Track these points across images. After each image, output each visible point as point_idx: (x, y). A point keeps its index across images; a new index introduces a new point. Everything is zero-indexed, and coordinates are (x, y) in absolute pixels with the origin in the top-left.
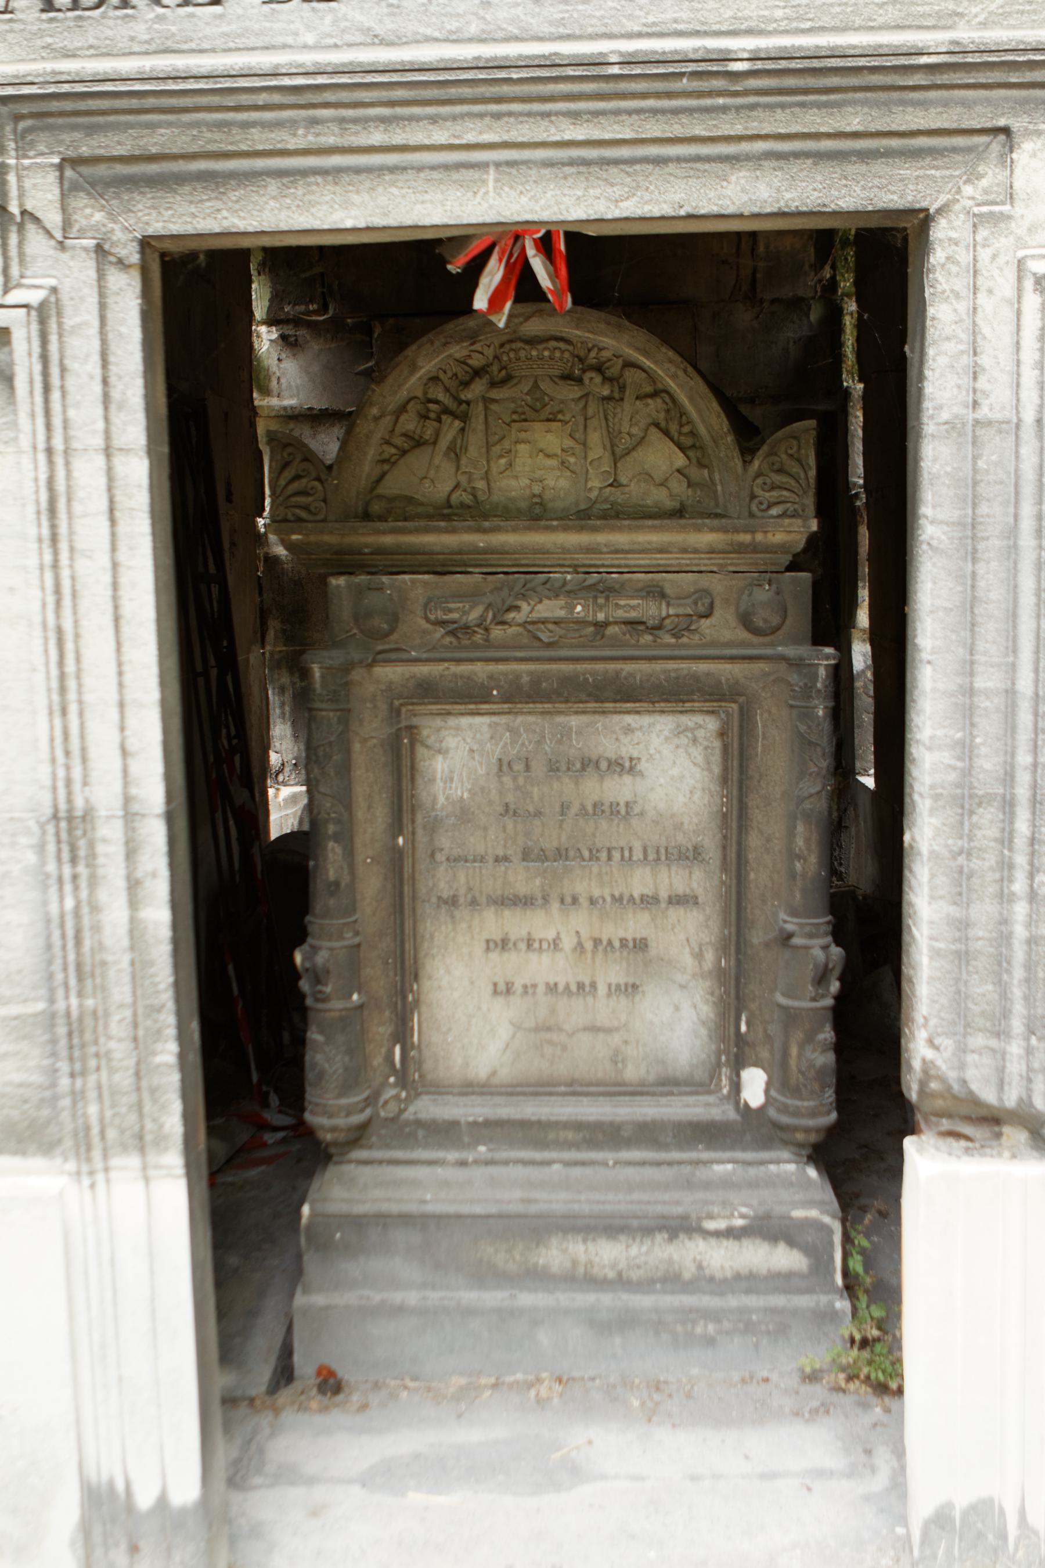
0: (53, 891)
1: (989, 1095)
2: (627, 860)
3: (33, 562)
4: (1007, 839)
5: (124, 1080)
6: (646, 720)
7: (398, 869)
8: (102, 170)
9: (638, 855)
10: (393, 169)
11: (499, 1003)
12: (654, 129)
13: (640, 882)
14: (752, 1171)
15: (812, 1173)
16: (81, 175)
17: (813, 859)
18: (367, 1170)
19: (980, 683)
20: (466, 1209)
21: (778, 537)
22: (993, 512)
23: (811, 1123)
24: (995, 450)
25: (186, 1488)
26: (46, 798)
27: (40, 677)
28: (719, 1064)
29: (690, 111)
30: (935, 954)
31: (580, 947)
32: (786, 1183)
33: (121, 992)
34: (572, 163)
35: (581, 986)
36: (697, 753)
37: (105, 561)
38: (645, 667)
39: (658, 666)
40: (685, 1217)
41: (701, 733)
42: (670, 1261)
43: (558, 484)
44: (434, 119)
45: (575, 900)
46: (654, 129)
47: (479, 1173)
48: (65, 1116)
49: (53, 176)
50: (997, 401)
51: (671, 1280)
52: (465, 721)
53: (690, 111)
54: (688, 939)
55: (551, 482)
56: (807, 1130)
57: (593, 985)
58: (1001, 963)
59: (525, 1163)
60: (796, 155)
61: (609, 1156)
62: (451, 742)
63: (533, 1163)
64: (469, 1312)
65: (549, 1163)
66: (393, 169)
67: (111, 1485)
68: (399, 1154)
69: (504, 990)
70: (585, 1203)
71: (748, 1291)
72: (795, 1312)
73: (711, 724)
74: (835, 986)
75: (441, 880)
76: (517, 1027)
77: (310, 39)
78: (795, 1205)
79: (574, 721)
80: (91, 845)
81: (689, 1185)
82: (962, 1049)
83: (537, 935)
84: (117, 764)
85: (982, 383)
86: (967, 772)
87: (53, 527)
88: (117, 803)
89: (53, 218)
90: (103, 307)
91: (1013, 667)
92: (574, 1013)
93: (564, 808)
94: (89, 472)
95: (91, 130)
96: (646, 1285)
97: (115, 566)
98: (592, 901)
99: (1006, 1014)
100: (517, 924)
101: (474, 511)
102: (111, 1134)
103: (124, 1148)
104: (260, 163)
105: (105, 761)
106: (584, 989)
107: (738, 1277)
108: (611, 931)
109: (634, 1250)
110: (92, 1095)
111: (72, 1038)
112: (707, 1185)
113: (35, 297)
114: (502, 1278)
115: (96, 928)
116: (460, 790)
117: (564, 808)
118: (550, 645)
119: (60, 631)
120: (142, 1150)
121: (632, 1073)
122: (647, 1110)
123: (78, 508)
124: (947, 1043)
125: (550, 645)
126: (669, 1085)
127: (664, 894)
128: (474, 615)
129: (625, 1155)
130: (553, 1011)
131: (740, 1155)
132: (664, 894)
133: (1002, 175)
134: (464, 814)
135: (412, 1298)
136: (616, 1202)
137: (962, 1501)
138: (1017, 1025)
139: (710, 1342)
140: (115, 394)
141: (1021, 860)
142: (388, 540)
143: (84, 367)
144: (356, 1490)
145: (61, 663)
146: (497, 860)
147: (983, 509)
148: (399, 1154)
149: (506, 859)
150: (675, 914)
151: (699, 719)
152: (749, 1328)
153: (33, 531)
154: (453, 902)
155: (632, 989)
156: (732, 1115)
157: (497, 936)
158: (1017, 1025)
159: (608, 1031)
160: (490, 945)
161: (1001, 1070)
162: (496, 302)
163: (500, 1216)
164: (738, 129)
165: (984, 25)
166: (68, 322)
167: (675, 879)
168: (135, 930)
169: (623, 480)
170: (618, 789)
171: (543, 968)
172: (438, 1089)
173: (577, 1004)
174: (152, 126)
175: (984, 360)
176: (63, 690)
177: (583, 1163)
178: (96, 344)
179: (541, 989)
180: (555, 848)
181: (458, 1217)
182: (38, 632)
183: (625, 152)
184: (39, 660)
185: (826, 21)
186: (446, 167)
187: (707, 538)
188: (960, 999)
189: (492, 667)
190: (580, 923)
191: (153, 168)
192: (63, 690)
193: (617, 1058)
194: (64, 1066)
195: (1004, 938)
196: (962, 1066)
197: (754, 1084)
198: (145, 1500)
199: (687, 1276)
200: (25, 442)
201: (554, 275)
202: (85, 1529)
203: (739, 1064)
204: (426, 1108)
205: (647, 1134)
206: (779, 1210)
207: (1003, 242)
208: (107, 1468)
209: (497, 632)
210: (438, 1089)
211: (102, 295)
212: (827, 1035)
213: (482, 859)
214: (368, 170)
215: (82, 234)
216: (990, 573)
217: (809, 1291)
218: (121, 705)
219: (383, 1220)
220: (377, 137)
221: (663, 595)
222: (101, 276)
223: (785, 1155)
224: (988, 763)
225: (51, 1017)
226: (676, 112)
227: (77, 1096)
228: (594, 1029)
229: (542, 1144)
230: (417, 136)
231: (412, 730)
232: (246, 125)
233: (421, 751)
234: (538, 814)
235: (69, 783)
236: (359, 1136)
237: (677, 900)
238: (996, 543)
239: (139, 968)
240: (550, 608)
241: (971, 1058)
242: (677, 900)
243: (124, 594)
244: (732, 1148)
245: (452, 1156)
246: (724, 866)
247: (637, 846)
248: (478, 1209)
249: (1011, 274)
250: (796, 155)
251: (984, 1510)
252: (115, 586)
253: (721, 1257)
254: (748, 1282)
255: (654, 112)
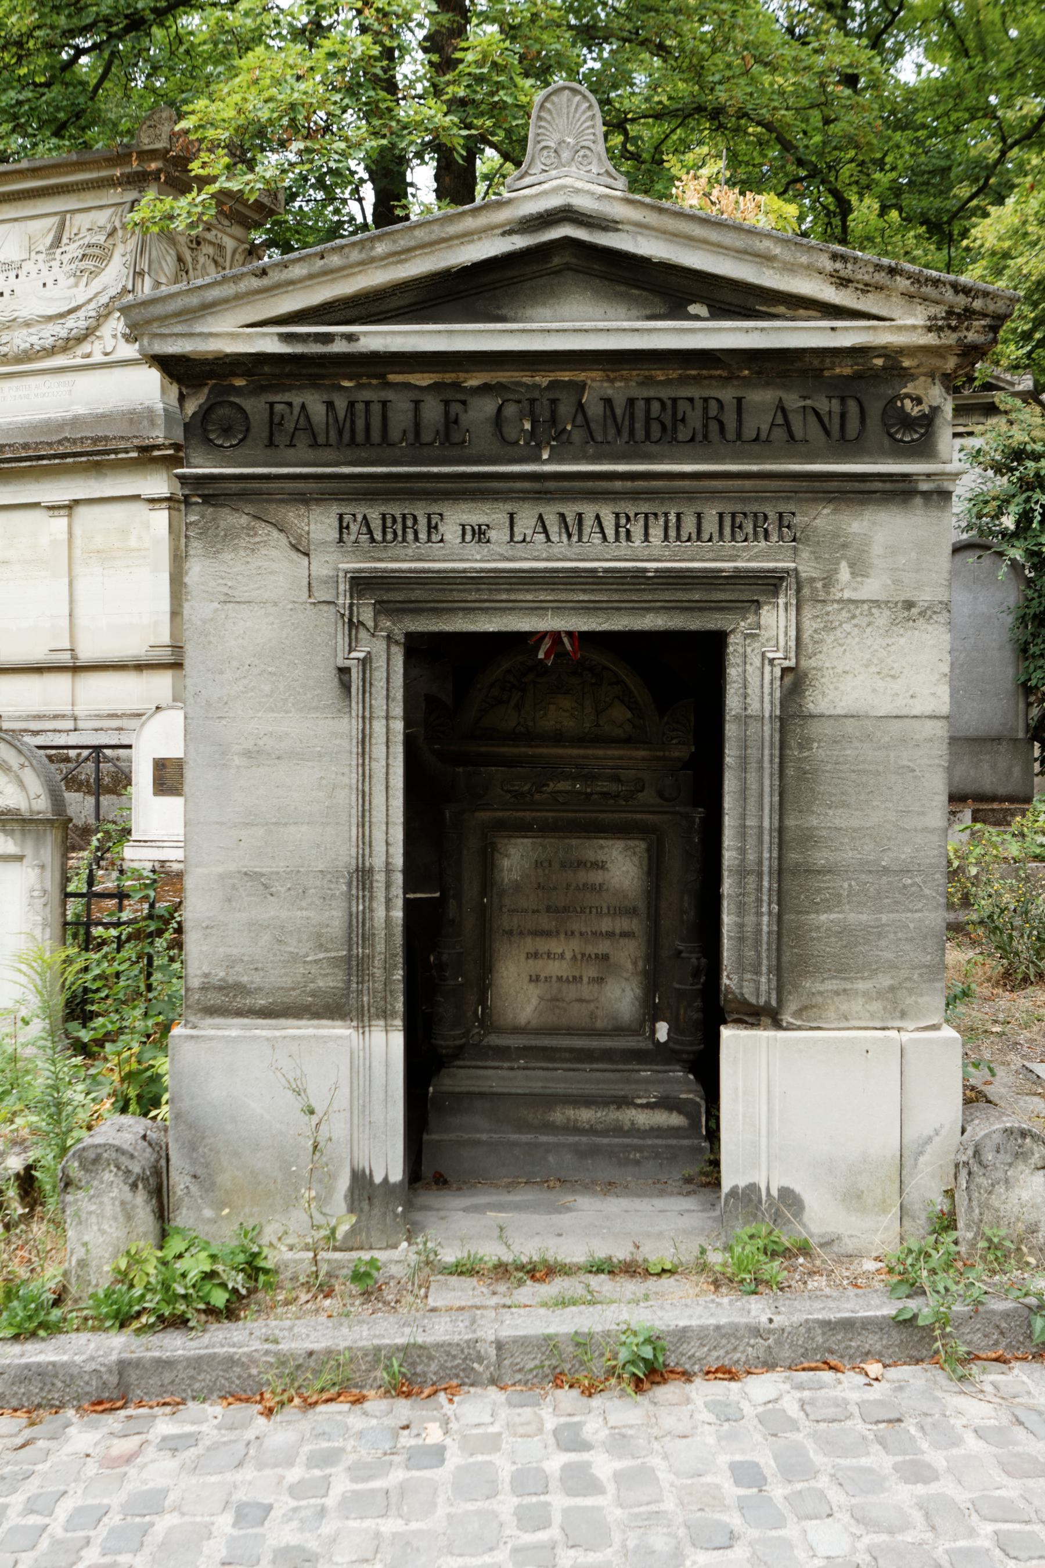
0: (354, 903)
1: (753, 1000)
2: (600, 914)
3: (354, 763)
4: (759, 889)
5: (379, 986)
6: (610, 842)
7: (484, 915)
8: (391, 606)
9: (605, 910)
10: (510, 609)
11: (532, 986)
12: (616, 597)
13: (606, 925)
14: (661, 1075)
15: (691, 1077)
16: (382, 608)
17: (692, 913)
18: (462, 1071)
19: (748, 823)
20: (513, 1091)
21: (676, 754)
22: (753, 752)
23: (690, 1048)
24: (753, 728)
25: (397, 1175)
26: (354, 862)
27: (354, 811)
28: (644, 1021)
29: (630, 590)
30: (730, 938)
31: (574, 958)
32: (677, 1080)
33: (380, 947)
34: (582, 608)
35: (574, 978)
36: (635, 859)
37: (384, 763)
38: (610, 815)
39: (616, 816)
40: (625, 1097)
41: (638, 850)
42: (618, 1120)
43: (568, 724)
44: (527, 590)
45: (573, 933)
46: (616, 597)
47: (520, 1073)
48: (353, 1002)
49: (371, 608)
50: (754, 708)
51: (618, 1130)
52: (519, 841)
53: (630, 590)
54: (628, 954)
55: (565, 723)
56: (688, 1053)
57: (581, 978)
58: (758, 942)
59: (543, 1069)
60: (673, 608)
61: (588, 1067)
62: (512, 851)
63: (548, 1069)
64: (514, 1144)
65: (556, 1069)
66: (510, 609)
67: (364, 1171)
68: (479, 1063)
69: (535, 979)
70: (574, 1089)
71: (657, 1137)
72: (681, 1147)
73: (643, 845)
74: (703, 979)
75: (506, 921)
76: (541, 998)
77: (478, 557)
78: (682, 1092)
79: (574, 842)
80: (371, 883)
81: (628, 1081)
82: (741, 980)
83: (553, 951)
84: (384, 849)
85: (748, 700)
86: (743, 860)
87: (363, 749)
88: (383, 866)
89: (370, 624)
90: (388, 659)
91: (762, 817)
92: (571, 992)
93: (568, 886)
94: (379, 727)
95: (388, 590)
96: (605, 1133)
97: (388, 765)
98: (581, 934)
99: (760, 964)
100: (543, 945)
101: (529, 737)
102: (373, 1010)
103: (378, 1017)
104: (456, 605)
105: (379, 848)
106: (576, 980)
107: (652, 1129)
108: (591, 950)
109: (599, 1114)
110: (365, 992)
111: (355, 966)
112: (638, 1082)
113: (361, 655)
114: (530, 1128)
115: (372, 919)
116: (515, 876)
117: (568, 886)
118: (564, 804)
119: (363, 791)
120: (385, 1018)
121: (599, 1024)
122: (607, 1043)
123: (374, 741)
124: (735, 977)
125: (564, 804)
126: (619, 1030)
127: (618, 931)
128: (526, 788)
129: (595, 1066)
130: (560, 990)
131: (655, 1067)
132: (618, 931)
133: (756, 619)
134: (517, 887)
135: (484, 1137)
136: (591, 1089)
137: (742, 1184)
138: (764, 969)
139: (637, 1163)
140: (392, 695)
141: (765, 898)
142: (483, 749)
143: (380, 684)
144: (461, 1213)
145: (363, 805)
146: (533, 912)
147: (749, 751)
148: (479, 1063)
149: (538, 911)
150: (623, 941)
151: (637, 842)
152: (657, 1156)
153: (355, 750)
154: (510, 933)
155: (600, 980)
156: (651, 1046)
157: (532, 951)
158: (764, 969)
159: (588, 1002)
160: (529, 955)
161: (758, 989)
162: (547, 654)
163: (531, 1095)
164: (650, 598)
165: (748, 560)
166: (374, 666)
167: (624, 924)
168: (388, 919)
169: (601, 723)
170: (596, 877)
171: (555, 968)
172: (500, 1031)
173: (573, 987)
174: (413, 590)
175: (749, 691)
176: (363, 816)
177: (573, 1070)
178: (385, 674)
179: (554, 979)
180: (564, 906)
181: (510, 1094)
182: (354, 792)
183: (604, 605)
184: (354, 804)
185: (685, 557)
186: (532, 609)
187: (642, 753)
188: (740, 958)
189: (534, 814)
190: (574, 946)
191: (412, 605)
192: (363, 816)
193: (592, 1016)
194: (354, 979)
195: (759, 932)
196: (741, 987)
197: (662, 1031)
198: (378, 1179)
199: (626, 1128)
200: (354, 714)
201: (572, 645)
202: (352, 1190)
203: (654, 1020)
204: (494, 1040)
205: (607, 1055)
206: (674, 1094)
207: (756, 645)
208: (363, 1164)
209: (537, 796)
210: (500, 1031)
211: (388, 655)
212: (698, 1003)
213: (526, 911)
214: (500, 609)
215: (381, 630)
216: (752, 778)
217: (688, 1137)
218: (387, 824)
219: (471, 1095)
220: (504, 597)
221: (620, 781)
222: (388, 647)
223: (678, 1068)
224: (751, 856)
225: (349, 958)
226: (625, 590)
227: (360, 992)
228: (580, 1000)
229: (553, 1060)
230: (521, 597)
231: (493, 845)
232: (451, 590)
233: (497, 855)
234: (555, 888)
235: (363, 855)
236: (458, 1053)
237: (624, 935)
238: (755, 765)
239: (389, 936)
240: (563, 786)
241: (745, 984)
242: (624, 935)
243: (391, 777)
244: (651, 1064)
245: (506, 1065)
246: (648, 918)
247: (605, 906)
248: (520, 1091)
249: (759, 657)
250: (673, 608)
251: (753, 1188)
252: (387, 773)
253: (643, 1118)
254: (657, 1131)
255: (616, 590)
